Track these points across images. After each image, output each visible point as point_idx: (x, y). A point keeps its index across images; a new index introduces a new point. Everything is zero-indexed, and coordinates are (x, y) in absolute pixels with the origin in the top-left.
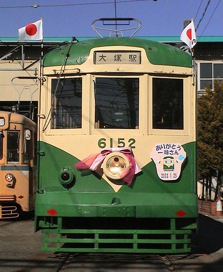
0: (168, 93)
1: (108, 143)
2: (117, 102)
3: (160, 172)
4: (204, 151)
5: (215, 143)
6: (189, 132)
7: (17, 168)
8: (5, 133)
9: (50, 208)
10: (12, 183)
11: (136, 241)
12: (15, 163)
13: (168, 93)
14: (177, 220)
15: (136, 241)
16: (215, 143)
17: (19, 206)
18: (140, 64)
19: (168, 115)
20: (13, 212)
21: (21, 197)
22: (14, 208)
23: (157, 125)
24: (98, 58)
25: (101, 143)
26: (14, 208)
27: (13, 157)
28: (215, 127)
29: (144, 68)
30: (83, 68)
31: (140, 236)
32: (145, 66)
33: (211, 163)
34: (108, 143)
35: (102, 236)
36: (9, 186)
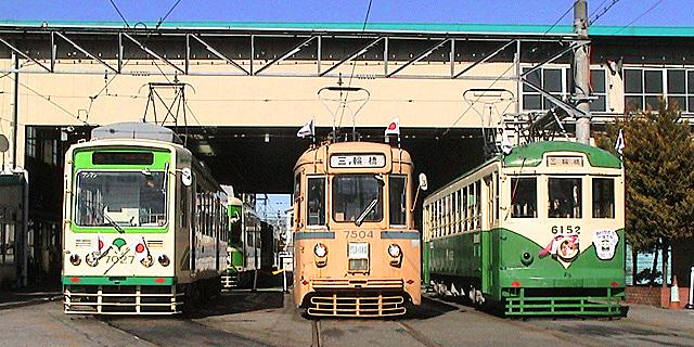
0: (603, 188)
1: (559, 229)
2: (564, 196)
3: (599, 251)
4: (651, 209)
5: (667, 196)
6: (619, 221)
7: (401, 235)
8: (386, 179)
9: (612, 281)
10: (398, 259)
11: (553, 305)
12: (400, 227)
13: (603, 188)
14: (612, 289)
15: (553, 305)
16: (667, 196)
17: (407, 296)
18: (581, 217)
19: (603, 206)
20: (399, 306)
21: (410, 282)
22: (311, 311)
23: (552, 213)
24: (550, 161)
25: (554, 229)
26: (311, 311)
27: (397, 217)
28: (670, 171)
29: (585, 171)
30: (539, 170)
31: (556, 302)
32: (587, 168)
33: (664, 226)
34: (559, 229)
35: (556, 302)
36: (394, 264)
